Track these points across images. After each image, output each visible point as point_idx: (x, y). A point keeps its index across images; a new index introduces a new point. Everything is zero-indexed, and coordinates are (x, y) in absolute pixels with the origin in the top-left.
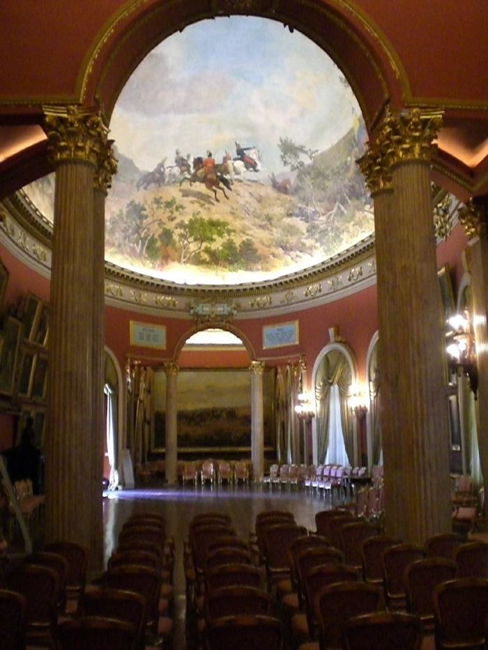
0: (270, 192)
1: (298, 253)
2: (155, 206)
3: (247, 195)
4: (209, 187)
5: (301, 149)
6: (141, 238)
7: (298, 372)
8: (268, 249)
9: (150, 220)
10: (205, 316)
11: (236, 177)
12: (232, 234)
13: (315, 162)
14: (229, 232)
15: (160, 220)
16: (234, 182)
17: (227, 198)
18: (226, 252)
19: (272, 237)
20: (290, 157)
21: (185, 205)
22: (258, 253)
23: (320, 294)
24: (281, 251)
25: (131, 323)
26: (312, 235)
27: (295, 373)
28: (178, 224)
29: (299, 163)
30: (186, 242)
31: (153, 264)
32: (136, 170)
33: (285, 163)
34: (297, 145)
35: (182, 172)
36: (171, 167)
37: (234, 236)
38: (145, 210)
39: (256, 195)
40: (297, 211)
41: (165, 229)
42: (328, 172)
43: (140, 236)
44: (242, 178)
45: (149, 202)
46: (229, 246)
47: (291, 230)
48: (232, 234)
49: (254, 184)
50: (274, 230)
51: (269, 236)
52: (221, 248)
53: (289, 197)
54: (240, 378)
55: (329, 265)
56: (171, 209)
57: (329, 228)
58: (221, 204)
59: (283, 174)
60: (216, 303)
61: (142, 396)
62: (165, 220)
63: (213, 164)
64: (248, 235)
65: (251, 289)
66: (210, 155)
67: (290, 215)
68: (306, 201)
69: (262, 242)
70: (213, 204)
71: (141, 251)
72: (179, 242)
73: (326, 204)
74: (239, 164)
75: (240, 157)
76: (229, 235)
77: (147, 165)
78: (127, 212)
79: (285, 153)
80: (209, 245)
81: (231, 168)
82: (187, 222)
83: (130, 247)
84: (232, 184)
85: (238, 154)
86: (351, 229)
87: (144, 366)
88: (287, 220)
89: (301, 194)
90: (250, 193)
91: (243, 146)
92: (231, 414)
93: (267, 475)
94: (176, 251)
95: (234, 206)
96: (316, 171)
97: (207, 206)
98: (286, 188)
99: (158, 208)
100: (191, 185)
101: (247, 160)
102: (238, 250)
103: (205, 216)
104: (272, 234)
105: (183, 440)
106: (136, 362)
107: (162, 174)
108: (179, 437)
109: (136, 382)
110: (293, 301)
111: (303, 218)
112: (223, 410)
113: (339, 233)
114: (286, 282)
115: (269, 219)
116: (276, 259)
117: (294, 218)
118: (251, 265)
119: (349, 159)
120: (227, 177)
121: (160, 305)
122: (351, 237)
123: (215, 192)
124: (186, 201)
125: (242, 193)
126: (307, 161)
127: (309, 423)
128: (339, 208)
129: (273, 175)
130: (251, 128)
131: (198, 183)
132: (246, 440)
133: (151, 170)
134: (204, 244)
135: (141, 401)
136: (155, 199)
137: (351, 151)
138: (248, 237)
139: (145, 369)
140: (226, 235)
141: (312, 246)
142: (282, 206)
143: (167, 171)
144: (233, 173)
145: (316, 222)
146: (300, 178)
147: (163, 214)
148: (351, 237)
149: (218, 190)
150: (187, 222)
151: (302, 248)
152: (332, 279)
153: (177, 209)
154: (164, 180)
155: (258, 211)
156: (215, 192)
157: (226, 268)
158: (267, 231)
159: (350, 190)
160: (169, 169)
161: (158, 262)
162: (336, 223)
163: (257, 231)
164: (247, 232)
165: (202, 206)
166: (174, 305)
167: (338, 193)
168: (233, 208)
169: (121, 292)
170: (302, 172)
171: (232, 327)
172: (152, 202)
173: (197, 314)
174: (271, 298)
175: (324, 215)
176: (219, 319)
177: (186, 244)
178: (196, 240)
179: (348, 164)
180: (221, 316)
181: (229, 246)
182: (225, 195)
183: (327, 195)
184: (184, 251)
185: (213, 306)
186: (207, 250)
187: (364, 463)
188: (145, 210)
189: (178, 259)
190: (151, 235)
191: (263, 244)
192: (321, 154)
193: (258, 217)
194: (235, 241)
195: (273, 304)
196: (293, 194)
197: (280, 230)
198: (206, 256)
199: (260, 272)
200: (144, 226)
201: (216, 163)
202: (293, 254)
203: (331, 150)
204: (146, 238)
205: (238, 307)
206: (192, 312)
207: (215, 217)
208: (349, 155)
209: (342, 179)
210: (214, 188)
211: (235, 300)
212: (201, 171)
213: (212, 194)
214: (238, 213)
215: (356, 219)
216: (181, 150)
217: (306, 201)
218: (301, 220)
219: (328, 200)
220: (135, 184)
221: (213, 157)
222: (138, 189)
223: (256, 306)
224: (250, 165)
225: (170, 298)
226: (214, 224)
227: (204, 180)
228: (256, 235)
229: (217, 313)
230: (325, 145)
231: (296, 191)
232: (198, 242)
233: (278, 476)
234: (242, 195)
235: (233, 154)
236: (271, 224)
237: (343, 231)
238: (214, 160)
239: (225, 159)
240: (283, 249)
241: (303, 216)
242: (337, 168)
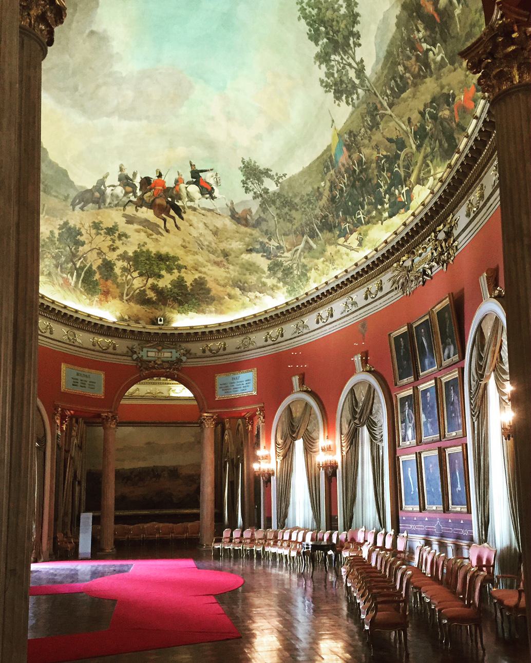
0: (228, 223)
1: (258, 294)
2: (93, 231)
3: (201, 225)
4: (158, 215)
5: (266, 173)
6: (76, 269)
7: (252, 426)
8: (222, 289)
9: (86, 248)
10: (150, 362)
11: (189, 204)
12: (183, 270)
13: (282, 188)
14: (179, 268)
15: (99, 249)
16: (188, 211)
17: (178, 228)
18: (176, 290)
19: (228, 275)
21: (129, 233)
22: (212, 294)
23: (282, 339)
24: (237, 291)
25: (63, 367)
26: (275, 273)
27: (250, 427)
28: (121, 255)
29: (263, 190)
30: (129, 277)
31: (90, 299)
32: (71, 184)
33: (247, 190)
34: (261, 168)
35: (126, 193)
36: (114, 186)
37: (186, 273)
38: (81, 235)
39: (211, 228)
40: (258, 247)
41: (104, 260)
42: (297, 200)
43: (75, 264)
44: (196, 206)
45: (87, 226)
46: (179, 284)
47: (251, 268)
48: (183, 270)
49: (209, 214)
50: (231, 267)
51: (225, 274)
52: (169, 286)
53: (249, 230)
54: (186, 435)
55: (294, 306)
56: (112, 237)
57: (295, 266)
58: (170, 236)
59: (243, 202)
60: (163, 348)
61: (73, 452)
62: (106, 250)
63: (164, 186)
64: (200, 272)
65: (203, 333)
66: (160, 176)
67: (250, 251)
68: (269, 235)
69: (216, 280)
70: (162, 235)
71: (77, 283)
72: (122, 276)
73: (292, 237)
74: (194, 189)
75: (194, 180)
76: (179, 272)
77: (85, 180)
78: (59, 234)
79: (248, 178)
80: (156, 282)
81: (184, 193)
82: (131, 254)
83: (63, 278)
85: (192, 177)
86: (321, 266)
87: (75, 418)
88: (246, 257)
89: (264, 226)
91: (198, 168)
92: (174, 473)
93: (219, 541)
94: (118, 287)
95: (187, 239)
96: (283, 200)
97: (155, 236)
98: (246, 220)
99: (98, 234)
100: (137, 210)
101: (203, 185)
102: (189, 289)
103: (152, 248)
104: (228, 272)
105: (120, 502)
106: (68, 413)
107: (103, 193)
108: (116, 500)
109: (68, 434)
110: (251, 347)
111: (265, 254)
112: (164, 469)
113: (306, 270)
114: (243, 326)
115: (226, 254)
116: (232, 301)
117: (254, 254)
118: (204, 306)
119: (323, 184)
120: (179, 203)
121: (97, 348)
122: (320, 275)
123: (165, 220)
124: (130, 229)
125: (195, 224)
126: (272, 186)
127: (268, 482)
128: (307, 242)
129: (232, 203)
130: (210, 145)
131: (144, 209)
132: (194, 499)
133: (90, 187)
134: (151, 281)
135: (71, 458)
136: (94, 222)
137: (326, 174)
138: (200, 275)
139: (77, 422)
140: (176, 271)
141: (274, 286)
142: (241, 241)
143: (109, 191)
144: (187, 200)
145: (280, 259)
146: (263, 207)
147: (103, 242)
148: (320, 275)
149: (168, 219)
150: (131, 254)
151: (263, 288)
152: (296, 322)
153: (120, 237)
154: (104, 201)
155: (213, 245)
156: (165, 220)
157: (174, 309)
158: (223, 269)
159: (321, 221)
160: (112, 188)
161: (96, 298)
162: (303, 260)
163: (211, 268)
164: (200, 269)
165: (149, 236)
166: (114, 348)
167: (307, 225)
168: (184, 241)
169: (51, 328)
170: (267, 200)
171: (181, 374)
172: (90, 227)
173: (139, 360)
174: (225, 344)
175: (289, 250)
176: (166, 365)
177: (130, 279)
178: (141, 275)
179: (321, 190)
180: (168, 362)
181: (179, 284)
182: (176, 226)
183: (294, 227)
184: (127, 287)
185: (159, 351)
186: (154, 288)
187: (332, 525)
188: (81, 235)
189: (119, 297)
190: (88, 265)
191: (218, 284)
192: (290, 178)
193: (213, 252)
194: (185, 279)
195: (228, 351)
196: (254, 226)
197: (237, 268)
198: (151, 295)
199: (214, 315)
200: (80, 254)
201: (167, 185)
202: (251, 295)
203: (302, 173)
204: (82, 268)
205: (188, 352)
206: (135, 356)
207: (164, 250)
208: (323, 180)
209: (312, 209)
210: (163, 215)
211: (184, 345)
212: (149, 194)
213: (161, 223)
214: (190, 246)
215: (328, 254)
216: (125, 166)
217: (269, 235)
218: (263, 256)
219: (295, 233)
220: (70, 200)
221: (163, 177)
222: (73, 210)
223: (208, 353)
224: (207, 191)
225: (110, 340)
226: (163, 259)
227: (151, 206)
228: (209, 272)
229: (164, 359)
230: (293, 169)
231: (257, 224)
232: (144, 278)
233: (231, 541)
234: (196, 225)
235: (187, 177)
236: (227, 260)
237: (311, 269)
238: (164, 182)
239: (177, 182)
240: (240, 290)
241: (264, 252)
242: (308, 195)
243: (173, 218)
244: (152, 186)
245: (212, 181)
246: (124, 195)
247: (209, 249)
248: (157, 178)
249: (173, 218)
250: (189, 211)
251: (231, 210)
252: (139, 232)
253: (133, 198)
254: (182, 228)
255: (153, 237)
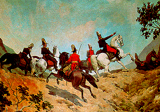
3: (113, 88)
4: (76, 86)
20: (151, 25)
36: (38, 58)
49: (119, 74)
66: (75, 51)
74: (103, 57)
75: (102, 48)
79: (145, 23)
81: (95, 64)
84: (98, 81)
90: (116, 85)
91: (104, 37)
99: (23, 98)
120: (93, 74)
143: (34, 61)
154: (30, 70)
182: (92, 95)
213: (79, 94)
227: (69, 78)
235: (96, 47)
239: (90, 53)
243: (89, 88)
244: (70, 60)
245: (116, 45)
246: (47, 68)
247: (124, 107)
248: (72, 53)
249: (89, 88)
250: (101, 79)
251: (136, 62)
252: (61, 103)
253: (54, 71)
254: (97, 96)
255: (73, 107)
